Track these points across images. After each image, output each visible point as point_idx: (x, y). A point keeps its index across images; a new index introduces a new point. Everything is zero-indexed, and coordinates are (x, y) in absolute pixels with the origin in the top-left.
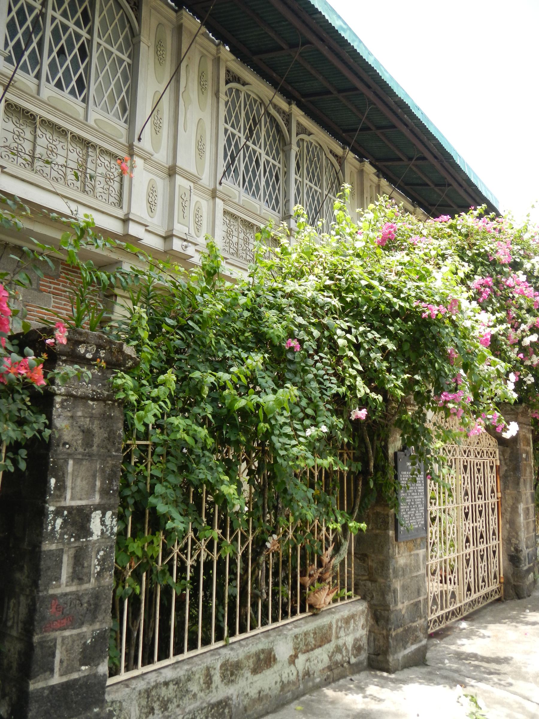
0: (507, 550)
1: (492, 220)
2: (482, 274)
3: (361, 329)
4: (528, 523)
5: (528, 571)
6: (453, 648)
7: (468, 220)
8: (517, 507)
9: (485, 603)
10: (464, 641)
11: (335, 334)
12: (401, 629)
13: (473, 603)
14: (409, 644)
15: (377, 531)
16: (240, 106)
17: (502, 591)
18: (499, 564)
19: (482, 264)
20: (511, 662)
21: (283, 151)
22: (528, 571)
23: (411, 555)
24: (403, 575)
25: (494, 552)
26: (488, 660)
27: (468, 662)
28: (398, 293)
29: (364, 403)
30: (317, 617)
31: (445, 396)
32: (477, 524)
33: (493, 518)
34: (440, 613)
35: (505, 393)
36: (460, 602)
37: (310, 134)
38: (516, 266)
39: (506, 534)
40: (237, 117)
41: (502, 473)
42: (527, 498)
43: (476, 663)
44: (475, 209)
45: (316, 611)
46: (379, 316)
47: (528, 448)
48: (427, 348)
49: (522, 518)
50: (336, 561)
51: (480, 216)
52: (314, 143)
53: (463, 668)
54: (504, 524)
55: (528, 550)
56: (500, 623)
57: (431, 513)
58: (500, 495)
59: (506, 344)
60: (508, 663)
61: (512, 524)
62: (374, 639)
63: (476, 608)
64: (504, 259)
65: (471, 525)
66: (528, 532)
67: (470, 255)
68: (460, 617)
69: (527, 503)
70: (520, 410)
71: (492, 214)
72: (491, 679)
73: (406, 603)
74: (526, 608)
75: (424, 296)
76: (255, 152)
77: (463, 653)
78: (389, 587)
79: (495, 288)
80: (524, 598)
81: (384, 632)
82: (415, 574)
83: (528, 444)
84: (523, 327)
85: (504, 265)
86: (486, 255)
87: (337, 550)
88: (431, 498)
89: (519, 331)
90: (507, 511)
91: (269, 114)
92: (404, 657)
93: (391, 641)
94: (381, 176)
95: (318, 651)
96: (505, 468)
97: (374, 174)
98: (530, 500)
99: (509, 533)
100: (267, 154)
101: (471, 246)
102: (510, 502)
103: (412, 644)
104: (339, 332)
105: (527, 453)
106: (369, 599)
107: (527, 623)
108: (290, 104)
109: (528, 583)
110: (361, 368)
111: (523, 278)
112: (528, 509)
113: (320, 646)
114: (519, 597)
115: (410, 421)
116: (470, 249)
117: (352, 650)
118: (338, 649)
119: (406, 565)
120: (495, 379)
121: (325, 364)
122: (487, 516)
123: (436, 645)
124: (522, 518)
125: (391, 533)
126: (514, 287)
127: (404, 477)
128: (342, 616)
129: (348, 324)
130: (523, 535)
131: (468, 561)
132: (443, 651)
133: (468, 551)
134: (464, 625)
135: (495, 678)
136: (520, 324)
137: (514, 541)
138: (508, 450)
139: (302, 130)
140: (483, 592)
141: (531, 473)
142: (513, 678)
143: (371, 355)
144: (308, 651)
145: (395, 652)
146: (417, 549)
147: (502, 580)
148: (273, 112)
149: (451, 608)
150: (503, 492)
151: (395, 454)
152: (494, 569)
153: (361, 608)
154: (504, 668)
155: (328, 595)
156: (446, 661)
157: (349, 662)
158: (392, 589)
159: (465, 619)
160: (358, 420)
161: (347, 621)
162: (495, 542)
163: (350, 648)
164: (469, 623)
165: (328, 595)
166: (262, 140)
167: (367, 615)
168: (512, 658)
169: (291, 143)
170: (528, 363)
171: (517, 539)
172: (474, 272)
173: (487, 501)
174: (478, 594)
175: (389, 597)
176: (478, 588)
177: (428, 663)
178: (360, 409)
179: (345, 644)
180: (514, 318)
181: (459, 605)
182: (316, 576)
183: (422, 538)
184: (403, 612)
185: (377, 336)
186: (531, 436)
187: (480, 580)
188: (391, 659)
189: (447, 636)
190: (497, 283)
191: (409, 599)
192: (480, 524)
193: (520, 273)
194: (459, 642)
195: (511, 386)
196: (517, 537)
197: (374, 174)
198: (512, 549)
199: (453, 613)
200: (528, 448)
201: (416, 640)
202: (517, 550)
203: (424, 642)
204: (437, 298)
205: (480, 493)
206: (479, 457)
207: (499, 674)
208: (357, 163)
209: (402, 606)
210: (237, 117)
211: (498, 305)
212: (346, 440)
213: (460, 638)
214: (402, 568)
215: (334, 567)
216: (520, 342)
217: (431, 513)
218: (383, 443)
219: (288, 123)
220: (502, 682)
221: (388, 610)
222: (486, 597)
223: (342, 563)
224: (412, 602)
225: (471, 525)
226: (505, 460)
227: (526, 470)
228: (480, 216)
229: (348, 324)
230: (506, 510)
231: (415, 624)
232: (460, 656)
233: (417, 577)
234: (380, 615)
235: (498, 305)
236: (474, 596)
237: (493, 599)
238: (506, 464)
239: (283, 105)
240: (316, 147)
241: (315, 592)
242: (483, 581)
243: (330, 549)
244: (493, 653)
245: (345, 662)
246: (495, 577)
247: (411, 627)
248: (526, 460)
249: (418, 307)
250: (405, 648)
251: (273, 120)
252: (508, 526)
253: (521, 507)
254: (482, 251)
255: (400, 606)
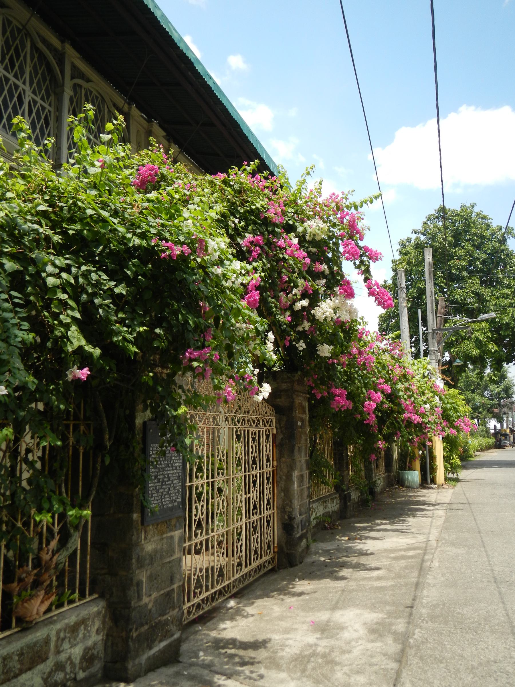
0: (281, 519)
1: (266, 178)
2: (254, 232)
3: (84, 268)
4: (302, 490)
5: (301, 538)
6: (214, 634)
7: (241, 176)
8: (292, 475)
9: (257, 576)
10: (228, 624)
11: (45, 271)
12: (146, 627)
13: (244, 577)
14: (157, 642)
15: (120, 515)
16: (25, 57)
17: (276, 561)
18: (273, 533)
19: (255, 223)
20: (268, 645)
21: (56, 94)
22: (301, 538)
23: (163, 539)
24: (151, 563)
25: (268, 522)
26: (245, 646)
27: (223, 651)
28: (132, 226)
29: (82, 358)
30: (28, 632)
31: (190, 353)
32: (251, 495)
33: (267, 488)
34: (204, 595)
35: (264, 354)
36: (229, 579)
37: (88, 81)
38: (290, 228)
39: (280, 502)
40: (21, 67)
41: (278, 441)
42: (301, 466)
43: (233, 651)
44: (248, 165)
45: (26, 625)
46: (116, 261)
47: (303, 416)
48: (173, 298)
49: (296, 486)
50: (63, 557)
51: (253, 174)
52: (94, 92)
53: (216, 660)
54: (279, 493)
55: (301, 517)
56: (268, 597)
57: (197, 488)
58: (275, 463)
59: (276, 307)
60: (265, 647)
61: (286, 493)
62: (112, 644)
63: (246, 583)
64: (277, 219)
65: (244, 496)
66: (302, 499)
67: (242, 211)
68: (227, 595)
69: (301, 470)
70: (296, 378)
71: (266, 173)
72: (243, 671)
73: (154, 595)
74: (296, 576)
75: (167, 235)
76: (17, 87)
77: (221, 640)
78: (131, 580)
79: (266, 247)
80: (297, 565)
81: (124, 634)
82: (168, 560)
83: (304, 412)
84: (295, 291)
85: (275, 225)
86: (256, 213)
87: (63, 542)
88: (218, 469)
89: (290, 295)
90: (281, 479)
91: (37, 50)
92: (149, 658)
93: (131, 644)
94: (171, 141)
95: (24, 677)
96: (281, 436)
97: (163, 137)
98: (304, 467)
99: (284, 501)
100: (34, 92)
101: (243, 203)
102: (285, 470)
103: (161, 641)
104: (50, 269)
105: (303, 421)
106: (108, 596)
107: (294, 595)
108: (63, 42)
109: (300, 550)
110: (78, 315)
111: (295, 241)
112: (302, 476)
113: (30, 669)
114: (292, 564)
115: (151, 383)
116: (242, 205)
117: (81, 662)
118: (59, 667)
119: (156, 551)
120: (254, 339)
121: (15, 305)
122: (261, 485)
123: (196, 632)
124: (296, 486)
125: (136, 516)
126: (285, 248)
127: (154, 449)
128: (67, 624)
129: (68, 262)
130: (296, 503)
131: (239, 534)
132: (202, 640)
133: (240, 524)
134: (232, 603)
135: (246, 669)
136: (292, 288)
137: (288, 509)
138: (285, 419)
139: (76, 73)
140: (254, 565)
141: (306, 440)
142: (266, 668)
143: (96, 301)
144: (9, 680)
145: (137, 655)
146: (172, 530)
147: (276, 550)
148: (40, 45)
149: (219, 587)
150: (279, 460)
151: (145, 423)
152: (267, 539)
153: (96, 609)
154: (262, 654)
155: (42, 602)
156: (201, 654)
157: (75, 679)
158: (135, 581)
159: (234, 596)
160: (77, 381)
161: (74, 629)
162: (269, 512)
163: (77, 661)
164: (237, 600)
165: (42, 602)
166: (27, 75)
167: (104, 617)
168: (270, 640)
169: (63, 85)
170: (300, 329)
171: (291, 507)
172: (245, 229)
173: (262, 471)
174: (249, 568)
175: (132, 592)
176: (249, 561)
177: (181, 659)
178: (81, 368)
179: (70, 658)
180: (286, 282)
181: (227, 583)
182: (31, 579)
183: (178, 518)
184: (150, 607)
185: (104, 277)
186: (307, 404)
187: (252, 554)
188: (130, 665)
189: (212, 618)
190: (270, 244)
191: (158, 589)
192: (254, 495)
193: (292, 235)
194: (222, 626)
195: (270, 346)
196: (291, 505)
197: (163, 137)
198: (286, 517)
199: (240, 581)
200: (303, 416)
201: (167, 634)
202: (291, 518)
203: (177, 636)
204: (182, 238)
205: (254, 462)
206: (254, 426)
207: (252, 664)
208: (145, 123)
209: (148, 600)
210: (21, 67)
211: (269, 266)
212: (62, 407)
213: (223, 620)
214: (150, 555)
215: (57, 564)
216: (291, 307)
217: (197, 488)
218: (127, 412)
219: (61, 62)
220: (254, 675)
221: (129, 608)
222: (259, 568)
223: (72, 557)
224: (162, 592)
225: (244, 496)
226: (281, 428)
227: (301, 437)
228: (253, 174)
229: (68, 262)
230: (281, 478)
231: (165, 617)
232: (219, 644)
233: (170, 562)
234: (119, 615)
235: (269, 266)
236: (245, 570)
237: (266, 570)
238: (282, 432)
239: (55, 42)
240: (97, 98)
241: (24, 601)
242: (256, 553)
243: (54, 544)
244: (254, 636)
245: (68, 680)
246: (269, 547)
247: (160, 621)
248: (301, 427)
249: (157, 245)
250: (151, 648)
251: (42, 57)
252: (282, 494)
253: (296, 474)
254: (254, 207)
255: (145, 600)
